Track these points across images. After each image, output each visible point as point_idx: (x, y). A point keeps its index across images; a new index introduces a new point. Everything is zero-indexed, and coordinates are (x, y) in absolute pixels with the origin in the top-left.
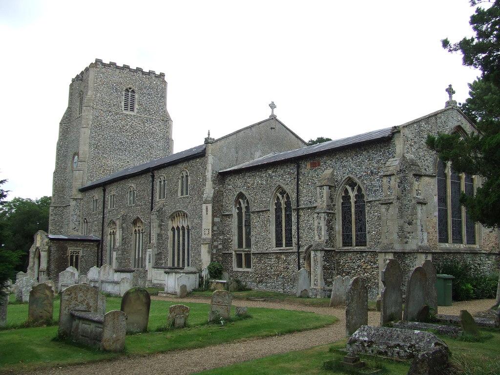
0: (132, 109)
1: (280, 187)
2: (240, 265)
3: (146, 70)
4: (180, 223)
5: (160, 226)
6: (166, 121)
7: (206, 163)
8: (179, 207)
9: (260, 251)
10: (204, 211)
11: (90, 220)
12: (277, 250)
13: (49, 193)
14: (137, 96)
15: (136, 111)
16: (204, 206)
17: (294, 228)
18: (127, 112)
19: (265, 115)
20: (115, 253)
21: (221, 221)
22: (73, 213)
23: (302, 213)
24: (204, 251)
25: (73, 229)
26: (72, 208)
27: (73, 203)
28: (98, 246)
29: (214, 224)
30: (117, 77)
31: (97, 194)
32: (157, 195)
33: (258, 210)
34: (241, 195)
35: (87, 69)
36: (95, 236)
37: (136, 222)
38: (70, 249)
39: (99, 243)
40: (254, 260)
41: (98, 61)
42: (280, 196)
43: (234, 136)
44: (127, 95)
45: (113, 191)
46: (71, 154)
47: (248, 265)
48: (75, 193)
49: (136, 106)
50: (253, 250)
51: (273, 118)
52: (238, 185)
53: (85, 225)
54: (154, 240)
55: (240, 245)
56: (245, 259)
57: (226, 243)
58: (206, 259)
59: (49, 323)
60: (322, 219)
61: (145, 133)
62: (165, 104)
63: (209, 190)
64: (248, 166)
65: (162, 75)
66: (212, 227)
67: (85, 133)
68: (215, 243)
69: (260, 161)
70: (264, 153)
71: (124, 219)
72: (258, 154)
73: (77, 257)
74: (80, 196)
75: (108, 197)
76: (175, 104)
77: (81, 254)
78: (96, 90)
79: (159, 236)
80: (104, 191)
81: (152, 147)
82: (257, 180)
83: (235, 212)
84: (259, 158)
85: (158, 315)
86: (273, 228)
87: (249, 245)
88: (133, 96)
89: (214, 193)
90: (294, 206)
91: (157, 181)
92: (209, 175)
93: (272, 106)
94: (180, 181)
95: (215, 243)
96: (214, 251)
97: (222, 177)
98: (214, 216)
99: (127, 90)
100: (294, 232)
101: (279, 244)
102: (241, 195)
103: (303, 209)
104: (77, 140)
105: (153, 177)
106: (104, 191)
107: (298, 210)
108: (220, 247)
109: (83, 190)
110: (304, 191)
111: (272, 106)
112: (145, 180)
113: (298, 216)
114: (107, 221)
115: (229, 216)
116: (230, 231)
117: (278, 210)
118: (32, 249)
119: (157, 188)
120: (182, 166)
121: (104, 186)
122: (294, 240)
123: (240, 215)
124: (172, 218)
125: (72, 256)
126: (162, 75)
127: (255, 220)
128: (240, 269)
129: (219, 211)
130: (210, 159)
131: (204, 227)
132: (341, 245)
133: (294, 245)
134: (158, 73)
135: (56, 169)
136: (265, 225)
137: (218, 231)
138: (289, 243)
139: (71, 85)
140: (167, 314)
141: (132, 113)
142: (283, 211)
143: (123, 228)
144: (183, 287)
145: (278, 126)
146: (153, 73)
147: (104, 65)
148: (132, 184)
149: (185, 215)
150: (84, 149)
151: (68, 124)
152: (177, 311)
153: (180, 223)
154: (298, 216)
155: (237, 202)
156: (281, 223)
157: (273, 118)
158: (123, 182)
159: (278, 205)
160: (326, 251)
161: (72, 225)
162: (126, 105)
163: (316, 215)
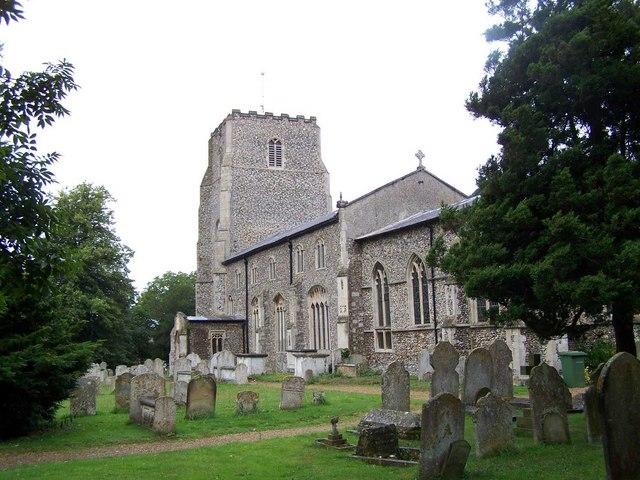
0: (279, 164)
1: (415, 255)
2: (381, 346)
3: (293, 115)
4: (319, 299)
5: (300, 303)
6: (321, 173)
7: (340, 230)
8: (317, 281)
9: (399, 328)
10: (339, 285)
11: (234, 297)
12: (412, 325)
13: (188, 265)
14: (283, 148)
15: (283, 165)
16: (339, 280)
17: (431, 301)
18: (274, 168)
21: (361, 295)
22: (216, 290)
23: (437, 284)
24: (341, 329)
25: (220, 308)
26: (215, 284)
27: (216, 279)
28: (243, 327)
29: (351, 299)
30: (258, 128)
31: (239, 268)
32: (296, 267)
33: (395, 282)
34: (379, 266)
35: (224, 124)
36: (240, 315)
37: (277, 299)
38: (211, 333)
39: (244, 324)
40: (394, 339)
41: (235, 114)
42: (416, 265)
43: (373, 196)
44: (271, 148)
45: (255, 263)
46: (214, 221)
47: (389, 346)
48: (217, 267)
49: (284, 160)
50: (393, 327)
51: (421, 169)
52: (373, 254)
53: (230, 304)
54: (293, 320)
55: (381, 323)
56: (386, 338)
57: (367, 320)
58: (343, 342)
59: (128, 411)
60: (453, 291)
61: (296, 190)
63: (344, 260)
64: (418, 221)
65: (313, 119)
66: (350, 303)
67: (224, 199)
68: (355, 322)
69: (406, 222)
70: (411, 212)
71: (266, 296)
72: (403, 215)
73: (220, 340)
74: (223, 270)
75: (250, 270)
76: (330, 153)
77: (224, 337)
78: (235, 145)
79: (299, 314)
80: (246, 263)
81: (305, 206)
82: (391, 248)
83: (373, 285)
84: (404, 219)
85: (226, 400)
86: (411, 302)
87: (389, 323)
88: (279, 149)
89: (350, 264)
90: (429, 277)
91: (295, 252)
92: (343, 243)
93: (420, 156)
94: (317, 251)
95: (355, 322)
96: (354, 330)
97: (360, 244)
98: (350, 290)
99: (271, 142)
100: (431, 307)
101: (418, 321)
102: (379, 266)
103: (438, 280)
104: (217, 206)
105: (291, 247)
106: (246, 263)
107: (433, 281)
108: (361, 325)
109: (227, 263)
111: (420, 156)
112: (284, 250)
113: (434, 289)
114: (250, 298)
115: (369, 289)
116: (370, 307)
117: (415, 282)
118: (173, 334)
119: (295, 259)
120: (317, 234)
121: (245, 258)
122: (431, 316)
123: (379, 287)
124: (311, 292)
125: (214, 340)
126: (313, 119)
127: (394, 294)
128: (382, 351)
129: (356, 285)
130: (344, 225)
131: (340, 303)
132: (476, 321)
133: (431, 321)
134: (307, 117)
135: (200, 240)
136: (403, 300)
137: (356, 306)
138: (427, 320)
139: (210, 141)
140: (113, 397)
141: (279, 168)
142: (420, 282)
143: (265, 306)
144: (309, 372)
145: (426, 179)
146: (302, 118)
147: (243, 116)
148: (272, 256)
149: (323, 290)
150: (224, 214)
151: (209, 183)
152: (245, 396)
154: (434, 289)
155: (375, 273)
156: (418, 297)
157: (421, 169)
158: (263, 253)
159: (415, 275)
160: (458, 328)
161: (216, 305)
162: (272, 159)
163: (446, 287)
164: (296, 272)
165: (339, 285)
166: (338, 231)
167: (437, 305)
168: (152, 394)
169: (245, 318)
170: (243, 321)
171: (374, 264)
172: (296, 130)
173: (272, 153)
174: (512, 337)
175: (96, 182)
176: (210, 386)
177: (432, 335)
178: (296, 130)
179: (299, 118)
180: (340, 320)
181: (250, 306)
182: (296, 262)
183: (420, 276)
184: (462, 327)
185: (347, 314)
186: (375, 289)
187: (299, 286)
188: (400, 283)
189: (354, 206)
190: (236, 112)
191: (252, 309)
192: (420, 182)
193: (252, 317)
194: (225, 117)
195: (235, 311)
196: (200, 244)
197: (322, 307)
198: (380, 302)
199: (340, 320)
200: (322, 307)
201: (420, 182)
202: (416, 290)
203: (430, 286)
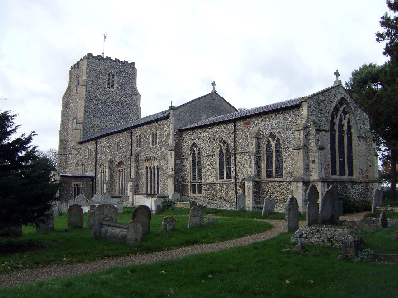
0: (113, 87)
6: (136, 95)
8: (151, 153)
9: (209, 182)
10: (169, 156)
14: (116, 78)
15: (115, 88)
16: (169, 152)
17: (232, 166)
19: (209, 91)
20: (105, 186)
21: (181, 162)
23: (238, 156)
28: (93, 181)
31: (91, 145)
32: (134, 145)
34: (194, 145)
38: (74, 184)
39: (93, 179)
40: (204, 188)
43: (189, 105)
45: (102, 143)
49: (116, 85)
52: (189, 138)
55: (194, 178)
56: (198, 189)
60: (253, 160)
62: (135, 84)
63: (171, 141)
65: (133, 64)
68: (177, 178)
70: (208, 116)
72: (204, 117)
73: (79, 188)
76: (142, 84)
77: (81, 186)
78: (88, 74)
79: (137, 173)
80: (96, 143)
81: (127, 113)
86: (217, 167)
87: (200, 179)
88: (113, 78)
92: (171, 131)
93: (214, 84)
94: (151, 136)
98: (176, 159)
99: (109, 74)
101: (222, 177)
103: (238, 153)
105: (132, 133)
107: (235, 154)
110: (239, 141)
111: (214, 84)
112: (231, 126)
124: (146, 161)
126: (133, 64)
131: (169, 167)
134: (130, 62)
135: (61, 129)
138: (229, 177)
139: (70, 72)
141: (113, 90)
148: (116, 138)
149: (155, 159)
153: (151, 164)
155: (192, 149)
157: (214, 93)
158: (109, 137)
159: (221, 151)
162: (109, 84)
163: (248, 157)
164: (135, 148)
165: (169, 156)
166: (168, 125)
167: (237, 168)
168: (109, 219)
169: (94, 175)
170: (92, 177)
171: (191, 144)
172: (123, 69)
173: (109, 81)
174: (297, 187)
175: (383, 55)
176: (147, 214)
177: (233, 186)
178: (123, 69)
179: (126, 62)
180: (170, 177)
181: (98, 168)
182: (135, 142)
183: (225, 152)
184: (258, 181)
185: (173, 173)
186: (191, 159)
187: (137, 157)
188: (210, 155)
189: (178, 110)
190: (90, 55)
191: (100, 170)
192: (213, 99)
193: (99, 176)
194: (82, 57)
195: (85, 171)
196: (61, 132)
197: (122, 172)
198: (194, 167)
199: (170, 177)
200: (122, 172)
201: (213, 99)
202: (221, 160)
203: (232, 158)
